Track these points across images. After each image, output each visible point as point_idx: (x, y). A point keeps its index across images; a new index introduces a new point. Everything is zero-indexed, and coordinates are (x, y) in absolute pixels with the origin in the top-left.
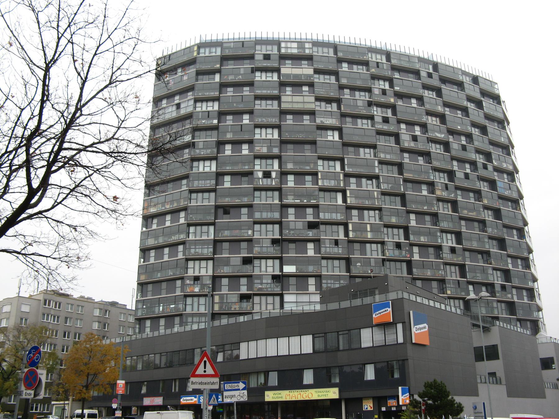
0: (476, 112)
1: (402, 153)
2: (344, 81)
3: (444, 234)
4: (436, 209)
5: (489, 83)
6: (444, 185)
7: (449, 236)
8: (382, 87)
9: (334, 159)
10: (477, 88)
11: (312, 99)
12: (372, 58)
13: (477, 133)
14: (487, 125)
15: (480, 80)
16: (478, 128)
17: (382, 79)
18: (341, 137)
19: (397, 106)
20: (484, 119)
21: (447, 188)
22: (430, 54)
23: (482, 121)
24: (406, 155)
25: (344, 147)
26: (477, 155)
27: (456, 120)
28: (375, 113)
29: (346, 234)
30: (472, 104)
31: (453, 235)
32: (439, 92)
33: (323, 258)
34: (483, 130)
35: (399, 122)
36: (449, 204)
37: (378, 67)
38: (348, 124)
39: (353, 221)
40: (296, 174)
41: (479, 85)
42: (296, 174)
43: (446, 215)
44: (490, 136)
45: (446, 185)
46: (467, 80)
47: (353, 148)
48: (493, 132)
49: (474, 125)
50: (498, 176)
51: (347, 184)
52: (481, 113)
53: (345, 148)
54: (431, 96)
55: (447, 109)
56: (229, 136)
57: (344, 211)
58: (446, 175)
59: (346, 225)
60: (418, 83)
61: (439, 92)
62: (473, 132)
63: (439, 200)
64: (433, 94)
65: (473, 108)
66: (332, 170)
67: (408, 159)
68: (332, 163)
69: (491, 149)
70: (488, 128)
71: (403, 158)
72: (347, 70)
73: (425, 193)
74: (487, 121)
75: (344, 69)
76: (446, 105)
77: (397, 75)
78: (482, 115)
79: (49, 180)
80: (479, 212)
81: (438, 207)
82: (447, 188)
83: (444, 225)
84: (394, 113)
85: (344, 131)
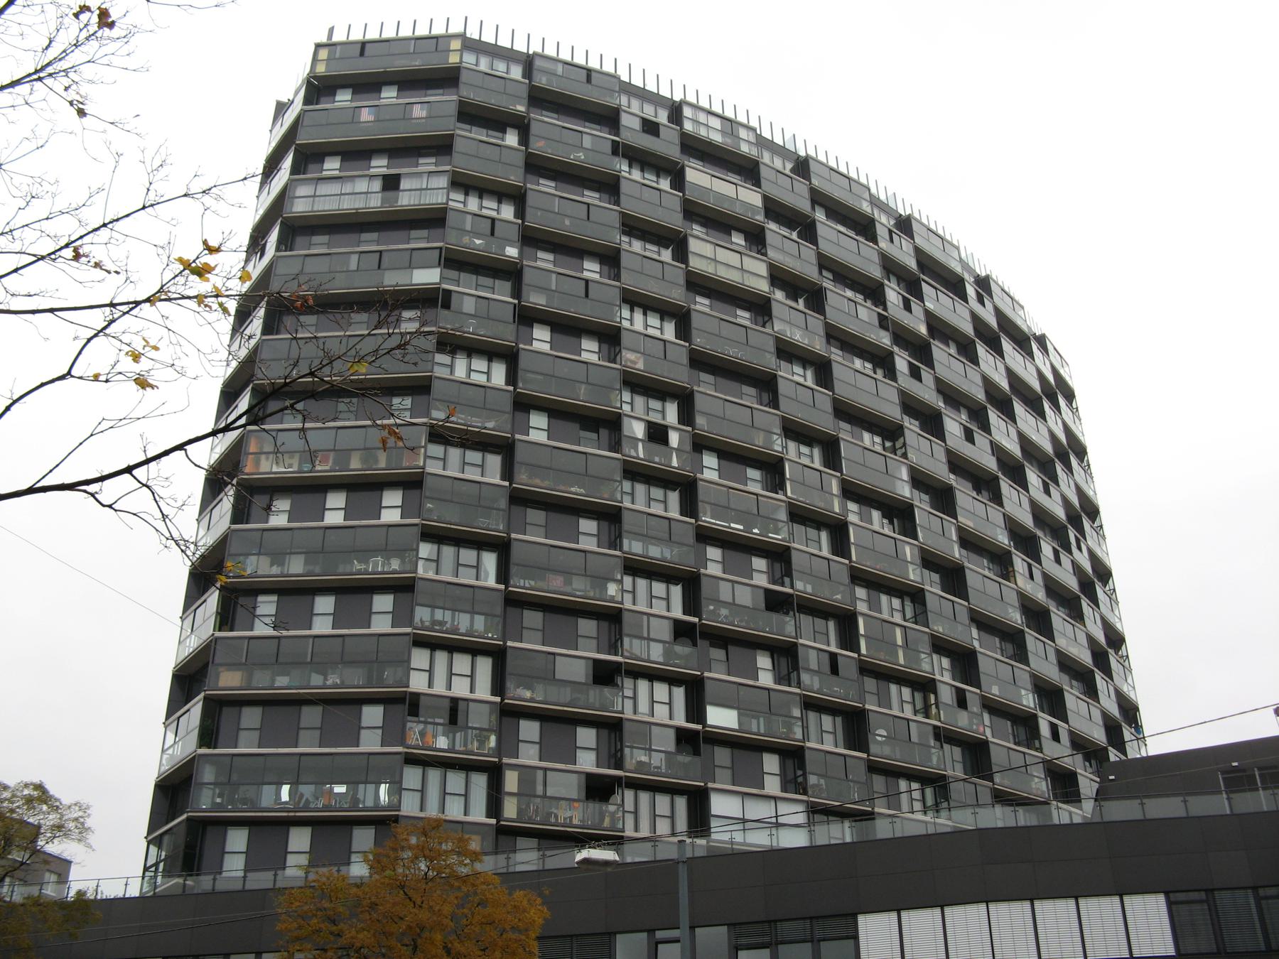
1: (702, 545)
2: (536, 299)
3: (812, 716)
4: (799, 735)
5: (938, 242)
6: (826, 658)
7: (827, 721)
8: (655, 418)
9: (480, 543)
10: (824, 400)
11: (443, 182)
12: (631, 320)
17: (655, 310)
18: (512, 378)
19: (694, 315)
21: (834, 669)
22: (788, 136)
23: (824, 420)
24: (714, 553)
25: (505, 719)
26: (926, 572)
27: (855, 378)
28: (626, 408)
29: (494, 807)
31: (839, 720)
32: (831, 450)
33: (420, 642)
34: (954, 579)
35: (700, 445)
36: (831, 624)
38: (533, 534)
39: (521, 761)
43: (828, 756)
45: (833, 657)
46: (884, 222)
47: (543, 513)
49: (940, 646)
50: (979, 640)
51: (509, 744)
53: (513, 611)
54: (806, 461)
55: (852, 506)
57: (499, 609)
58: (839, 720)
59: (495, 773)
60: (769, 419)
61: (831, 450)
63: (811, 705)
64: (811, 457)
66: (467, 578)
67: (720, 566)
68: (468, 555)
69: (974, 638)
70: (980, 657)
71: (704, 561)
72: (546, 347)
73: (766, 679)
75: (537, 345)
76: (851, 491)
77: (702, 304)
81: (805, 728)
82: (834, 669)
83: (812, 682)
84: (687, 416)
85: (516, 553)
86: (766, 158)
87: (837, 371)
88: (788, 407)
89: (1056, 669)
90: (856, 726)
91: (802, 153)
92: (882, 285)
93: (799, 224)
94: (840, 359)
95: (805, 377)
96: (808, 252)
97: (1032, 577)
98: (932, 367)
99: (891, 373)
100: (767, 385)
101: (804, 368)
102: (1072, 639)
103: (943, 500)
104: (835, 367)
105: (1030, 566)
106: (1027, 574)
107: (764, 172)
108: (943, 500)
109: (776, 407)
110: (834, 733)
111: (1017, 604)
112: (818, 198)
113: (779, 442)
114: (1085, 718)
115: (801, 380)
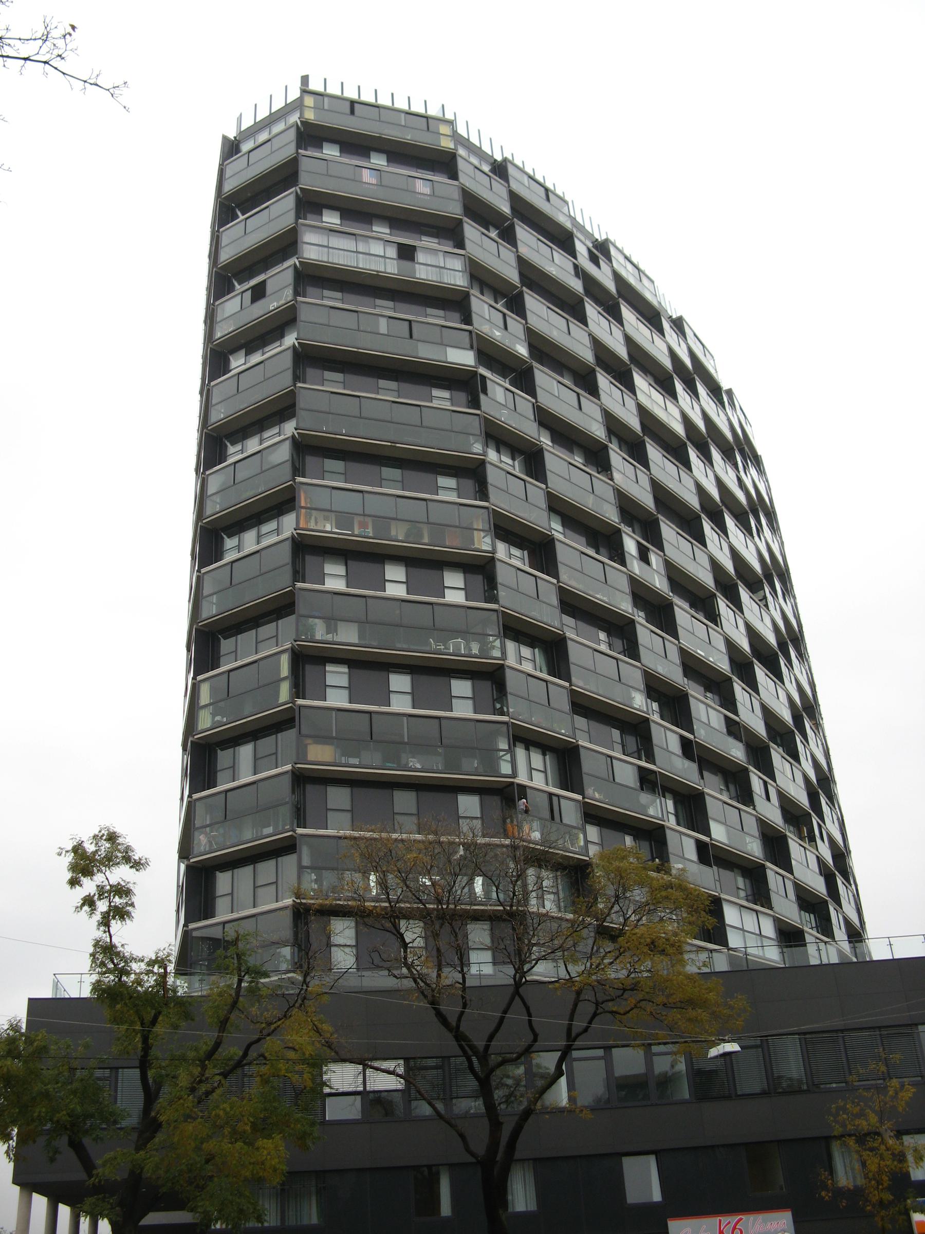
0: (527, 584)
10: (537, 492)
13: (527, 667)
14: (570, 634)
15: (511, 170)
16: (532, 645)
20: (545, 514)
23: (547, 614)
30: (516, 552)
34: (675, 706)
37: (352, 112)
40: (357, 662)
41: (545, 481)
42: (357, 662)
44: (564, 577)
48: (589, 664)
49: (507, 530)
52: (547, 585)
56: (347, 636)
62: (511, 661)
65: (518, 564)
74: (569, 620)
78: (562, 701)
79: (312, 455)
80: (490, 758)
81: (513, 763)
86: (462, 152)
87: (575, 653)
88: (498, 500)
89: (795, 907)
90: (567, 761)
91: (499, 158)
92: (606, 447)
93: (513, 370)
94: (561, 537)
95: (514, 467)
96: (525, 403)
97: (768, 799)
98: (662, 549)
99: (619, 555)
100: (473, 473)
101: (513, 459)
102: (776, 696)
103: (662, 616)
104: (572, 648)
105: (765, 783)
106: (764, 796)
107: (461, 164)
108: (662, 616)
109: (493, 599)
110: (545, 772)
111: (757, 834)
112: (518, 203)
113: (497, 643)
114: (806, 864)
115: (510, 470)
